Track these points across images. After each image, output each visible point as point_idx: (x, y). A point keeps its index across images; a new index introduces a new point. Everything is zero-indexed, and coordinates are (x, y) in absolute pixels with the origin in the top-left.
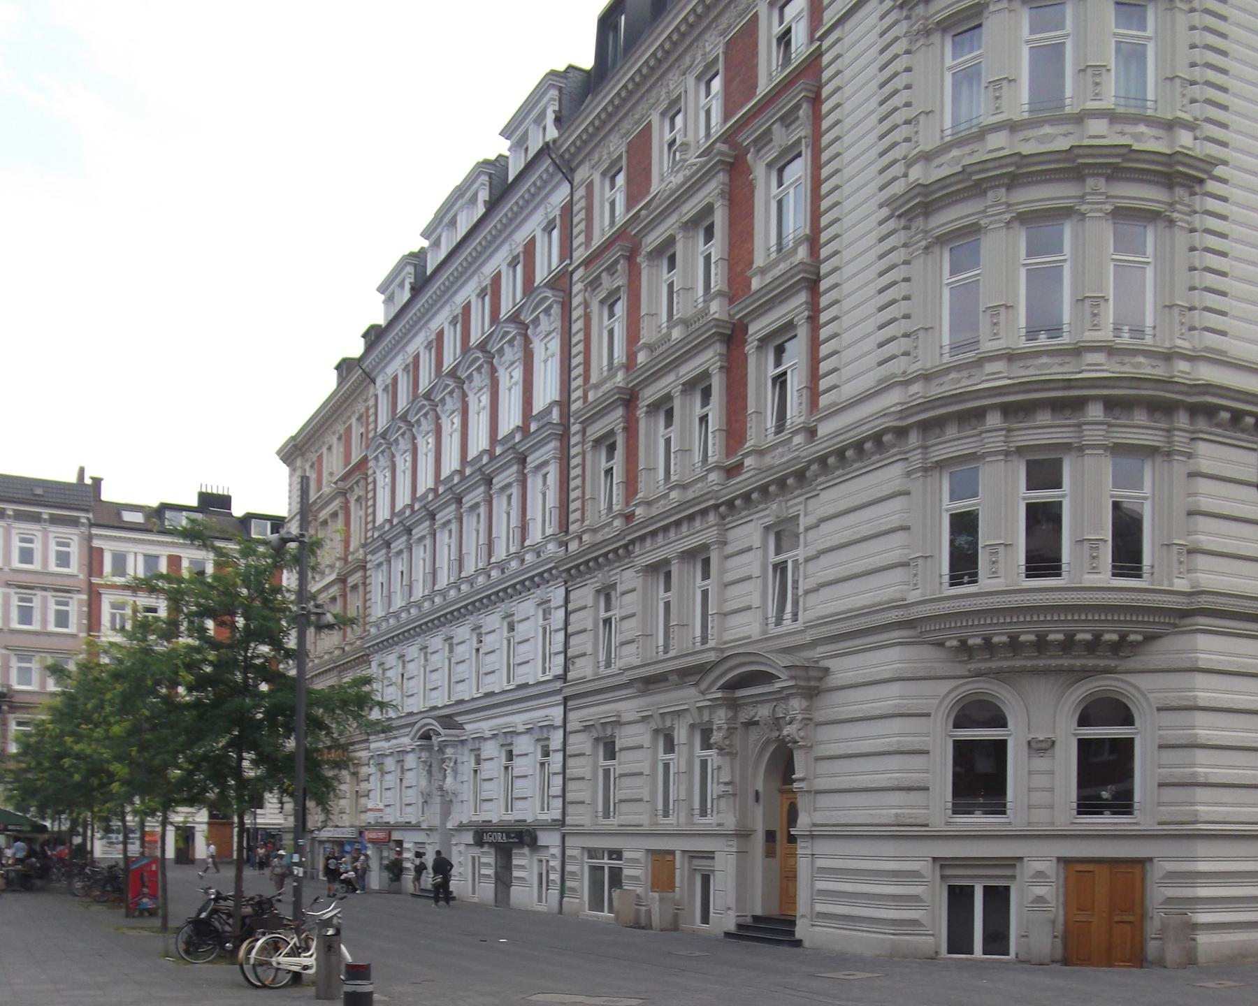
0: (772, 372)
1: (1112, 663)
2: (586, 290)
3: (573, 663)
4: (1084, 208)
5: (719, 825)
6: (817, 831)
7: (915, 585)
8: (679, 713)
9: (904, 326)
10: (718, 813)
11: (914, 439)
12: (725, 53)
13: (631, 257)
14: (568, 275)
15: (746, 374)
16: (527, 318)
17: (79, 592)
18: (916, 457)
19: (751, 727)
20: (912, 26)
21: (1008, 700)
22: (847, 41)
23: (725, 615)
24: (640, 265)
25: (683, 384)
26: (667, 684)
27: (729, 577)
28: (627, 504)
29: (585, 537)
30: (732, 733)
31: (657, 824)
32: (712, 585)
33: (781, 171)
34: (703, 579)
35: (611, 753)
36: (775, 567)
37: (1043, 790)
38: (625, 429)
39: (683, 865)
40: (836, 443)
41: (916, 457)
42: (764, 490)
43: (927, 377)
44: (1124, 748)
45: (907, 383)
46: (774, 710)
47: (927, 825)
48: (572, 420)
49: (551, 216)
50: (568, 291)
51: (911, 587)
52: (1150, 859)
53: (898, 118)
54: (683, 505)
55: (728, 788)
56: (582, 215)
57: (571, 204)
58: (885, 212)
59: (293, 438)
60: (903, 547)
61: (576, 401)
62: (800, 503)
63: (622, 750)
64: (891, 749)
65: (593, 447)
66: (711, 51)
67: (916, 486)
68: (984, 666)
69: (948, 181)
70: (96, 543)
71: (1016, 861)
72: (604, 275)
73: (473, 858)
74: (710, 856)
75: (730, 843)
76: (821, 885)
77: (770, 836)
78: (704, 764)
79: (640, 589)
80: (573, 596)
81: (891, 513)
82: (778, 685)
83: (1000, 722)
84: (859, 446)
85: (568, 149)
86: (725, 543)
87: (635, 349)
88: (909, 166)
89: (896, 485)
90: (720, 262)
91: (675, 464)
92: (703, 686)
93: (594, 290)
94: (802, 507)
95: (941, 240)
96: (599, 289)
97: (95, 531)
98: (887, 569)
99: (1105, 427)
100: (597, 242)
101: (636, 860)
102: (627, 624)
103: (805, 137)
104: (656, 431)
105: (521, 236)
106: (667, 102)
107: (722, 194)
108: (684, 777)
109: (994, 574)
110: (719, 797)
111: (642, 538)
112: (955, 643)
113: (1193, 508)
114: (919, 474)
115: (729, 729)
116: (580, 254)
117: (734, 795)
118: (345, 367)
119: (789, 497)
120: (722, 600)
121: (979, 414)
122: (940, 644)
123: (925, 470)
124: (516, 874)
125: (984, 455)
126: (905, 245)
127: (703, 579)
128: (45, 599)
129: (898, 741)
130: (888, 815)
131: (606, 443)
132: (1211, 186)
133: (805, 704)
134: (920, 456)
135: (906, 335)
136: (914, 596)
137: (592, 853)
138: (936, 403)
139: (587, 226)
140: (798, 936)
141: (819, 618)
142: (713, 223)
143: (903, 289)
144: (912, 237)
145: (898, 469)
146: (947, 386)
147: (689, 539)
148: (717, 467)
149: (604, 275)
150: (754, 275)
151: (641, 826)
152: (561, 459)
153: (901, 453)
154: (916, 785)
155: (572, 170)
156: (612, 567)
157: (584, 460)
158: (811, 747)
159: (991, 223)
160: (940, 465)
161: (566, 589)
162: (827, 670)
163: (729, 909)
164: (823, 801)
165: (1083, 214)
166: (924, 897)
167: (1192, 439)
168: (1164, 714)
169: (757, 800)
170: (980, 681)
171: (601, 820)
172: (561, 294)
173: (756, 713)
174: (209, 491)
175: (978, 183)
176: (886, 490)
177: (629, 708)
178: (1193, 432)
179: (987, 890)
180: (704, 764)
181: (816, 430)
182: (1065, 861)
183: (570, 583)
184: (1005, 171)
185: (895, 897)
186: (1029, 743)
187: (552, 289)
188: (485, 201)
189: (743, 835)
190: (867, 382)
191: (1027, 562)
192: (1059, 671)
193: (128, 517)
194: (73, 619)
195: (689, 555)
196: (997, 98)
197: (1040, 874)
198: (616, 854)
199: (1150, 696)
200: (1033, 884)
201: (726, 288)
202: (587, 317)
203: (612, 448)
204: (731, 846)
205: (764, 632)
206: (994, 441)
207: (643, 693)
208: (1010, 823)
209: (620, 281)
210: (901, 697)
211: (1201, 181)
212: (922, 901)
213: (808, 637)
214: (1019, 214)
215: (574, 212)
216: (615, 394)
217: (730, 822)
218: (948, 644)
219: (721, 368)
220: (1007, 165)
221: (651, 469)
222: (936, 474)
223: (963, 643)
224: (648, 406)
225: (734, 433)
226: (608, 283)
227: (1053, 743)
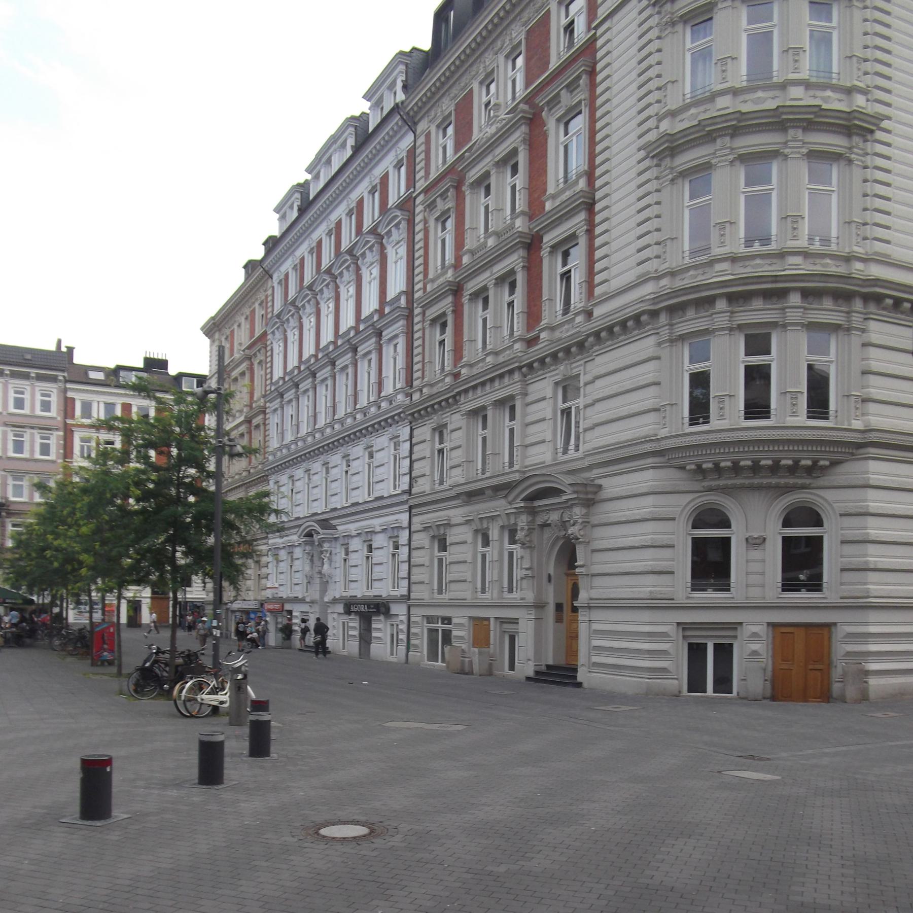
0: (560, 270)
1: (808, 481)
2: (425, 211)
3: (416, 482)
4: (786, 151)
6: (593, 603)
8: (493, 518)
9: (656, 236)
10: (521, 590)
11: (663, 319)
12: (526, 39)
13: (458, 187)
15: (542, 272)
16: (382, 231)
17: (57, 430)
18: (665, 332)
19: (545, 528)
20: (662, 19)
21: (732, 508)
22: (615, 30)
23: (526, 446)
24: (464, 192)
25: (496, 279)
26: (484, 497)
28: (455, 366)
29: (425, 390)
30: (531, 533)
31: (477, 598)
32: (517, 424)
33: (567, 124)
34: (510, 421)
35: (443, 547)
36: (563, 411)
39: (495, 628)
40: (607, 322)
41: (665, 332)
42: (554, 356)
43: (673, 274)
44: (816, 543)
45: (658, 278)
47: (673, 599)
48: (415, 305)
50: (412, 211)
51: (661, 426)
52: (835, 624)
54: (496, 367)
55: (529, 572)
57: (414, 148)
58: (642, 154)
59: (213, 318)
60: (656, 397)
62: (581, 365)
64: (646, 544)
65: (430, 324)
66: (516, 37)
67: (665, 353)
69: (688, 132)
70: (70, 394)
72: (438, 200)
73: (344, 623)
74: (515, 621)
75: (530, 612)
76: (596, 643)
77: (559, 607)
78: (511, 554)
79: (464, 427)
80: (416, 432)
81: (647, 372)
82: (564, 498)
83: (726, 524)
84: (623, 324)
85: (412, 108)
86: (526, 394)
87: (461, 253)
89: (650, 352)
90: (522, 191)
91: (490, 337)
93: (431, 210)
94: (582, 368)
95: (683, 174)
96: (435, 210)
97: (69, 386)
99: (802, 310)
100: (433, 176)
102: (455, 453)
104: (476, 313)
106: (484, 74)
107: (524, 141)
108: (496, 565)
109: (722, 417)
110: (522, 579)
111: (466, 391)
112: (693, 467)
113: (866, 369)
115: (529, 529)
116: (421, 185)
117: (533, 577)
118: (250, 266)
119: (572, 361)
120: (524, 436)
121: (710, 301)
122: (682, 468)
124: (374, 634)
125: (714, 331)
126: (657, 178)
127: (510, 421)
128: (32, 435)
130: (645, 592)
131: (440, 322)
132: (879, 135)
133: (584, 511)
134: (667, 331)
135: (658, 243)
136: (663, 433)
137: (430, 619)
138: (680, 293)
139: (426, 164)
140: (579, 679)
141: (594, 449)
142: (517, 162)
143: (655, 210)
144: (662, 172)
145: (651, 341)
146: (687, 280)
147: (500, 391)
148: (521, 339)
149: (438, 200)
150: (548, 199)
151: (465, 599)
152: (407, 333)
155: (415, 124)
158: (589, 542)
159: (719, 162)
160: (682, 338)
161: (411, 427)
162: (600, 486)
163: (529, 660)
164: (598, 581)
166: (671, 651)
167: (865, 319)
168: (845, 519)
169: (550, 581)
170: (711, 495)
171: (436, 596)
172: (407, 213)
174: (152, 356)
175: (710, 133)
176: (643, 356)
177: (457, 514)
178: (866, 314)
180: (511, 554)
181: (592, 312)
182: (773, 625)
183: (413, 424)
184: (729, 124)
185: (649, 652)
186: (747, 539)
187: (401, 210)
188: (352, 146)
189: (539, 606)
190: (630, 277)
191: (745, 408)
192: (769, 487)
193: (93, 375)
194: (53, 449)
195: (500, 403)
197: (755, 635)
198: (447, 620)
199: (835, 505)
200: (750, 642)
201: (527, 209)
202: (426, 231)
203: (444, 326)
204: (530, 614)
205: (555, 459)
206: (722, 320)
207: (467, 503)
208: (733, 598)
209: (450, 204)
210: (654, 506)
211: (872, 132)
212: (669, 654)
213: (586, 463)
218: (688, 467)
219: (523, 267)
220: (731, 120)
221: (473, 341)
222: (680, 344)
223: (699, 467)
224: (470, 295)
225: (533, 315)
226: (441, 206)
227: (764, 539)
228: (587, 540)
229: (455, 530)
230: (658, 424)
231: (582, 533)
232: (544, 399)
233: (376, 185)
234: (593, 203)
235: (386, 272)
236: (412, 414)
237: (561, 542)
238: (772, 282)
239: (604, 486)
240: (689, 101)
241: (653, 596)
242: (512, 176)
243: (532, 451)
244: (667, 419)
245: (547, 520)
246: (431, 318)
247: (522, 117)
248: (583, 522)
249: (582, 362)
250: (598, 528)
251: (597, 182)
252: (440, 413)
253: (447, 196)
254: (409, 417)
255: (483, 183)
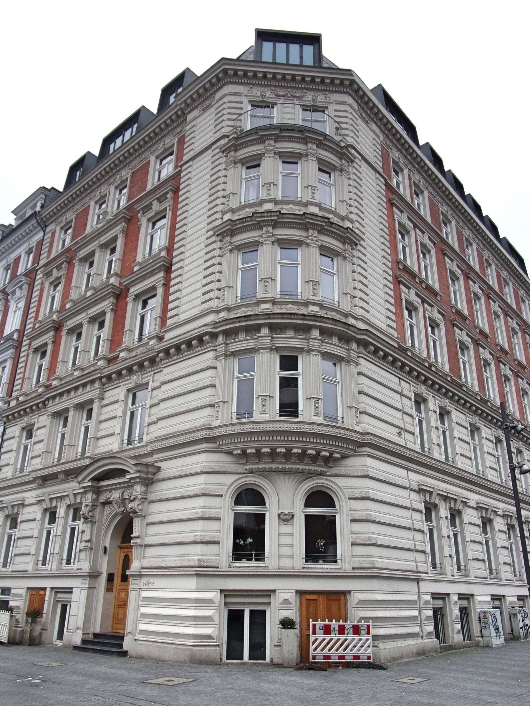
1: (325, 470)
2: (44, 277)
4: (308, 241)
5: (78, 570)
7: (217, 417)
8: (61, 498)
9: (217, 285)
10: (79, 561)
11: (221, 339)
12: (131, 177)
14: (35, 272)
15: (126, 313)
16: (9, 290)
20: (227, 160)
22: (194, 167)
23: (98, 439)
24: (74, 264)
25: (90, 318)
26: (56, 480)
27: (102, 417)
28: (48, 380)
31: (37, 570)
32: (92, 423)
33: (154, 224)
37: (286, 545)
38: (53, 342)
39: (50, 598)
40: (176, 341)
41: (221, 349)
43: (229, 309)
44: (331, 522)
45: (218, 312)
46: (123, 494)
47: (218, 567)
48: (25, 338)
49: (31, 246)
50: (33, 279)
51: (214, 419)
52: (349, 592)
53: (220, 194)
55: (88, 544)
56: (36, 304)
57: (43, 240)
58: (211, 233)
60: (211, 396)
61: (22, 357)
62: (151, 375)
63: (21, 522)
64: (197, 516)
65: (33, 352)
66: (168, 143)
67: (220, 364)
68: (254, 467)
71: (269, 593)
72: (54, 270)
74: (69, 591)
75: (84, 582)
77: (111, 577)
78: (73, 530)
79: (48, 427)
80: (7, 431)
81: (206, 377)
84: (189, 343)
85: (45, 216)
86: (103, 399)
87: (65, 302)
88: (223, 215)
89: (209, 363)
90: (117, 261)
91: (79, 358)
92: (80, 478)
93: (48, 277)
94: (151, 378)
95: (238, 248)
98: (202, 408)
99: (320, 342)
100: (53, 255)
101: (20, 595)
102: (37, 446)
103: (169, 206)
105: (14, 256)
106: (99, 196)
107: (123, 231)
108: (59, 539)
109: (264, 412)
110: (80, 551)
111: (54, 397)
112: (239, 452)
113: (361, 390)
114: (223, 357)
115: (92, 506)
116: (42, 263)
117: (91, 549)
121: (257, 328)
122: (230, 453)
123: (226, 356)
125: (259, 349)
126: (220, 248)
127: (87, 420)
129: (202, 511)
131: (41, 351)
132: (359, 247)
133: (144, 489)
134: (224, 348)
135: (219, 289)
138: (235, 320)
139: (49, 250)
140: (125, 648)
142: (116, 246)
143: (218, 268)
144: (223, 245)
145: (211, 355)
146: (241, 313)
147: (82, 397)
148: (104, 358)
149: (54, 270)
151: (26, 571)
152: (14, 359)
153: (212, 347)
154: (212, 540)
155: (46, 226)
156: (34, 414)
157: (25, 370)
158: (145, 516)
160: (234, 354)
161: (5, 427)
162: (159, 468)
163: (78, 628)
164: (150, 552)
165: (308, 244)
167: (358, 357)
168: (353, 502)
169: (105, 552)
170: (251, 476)
171: (64, 566)
172: (30, 280)
173: (111, 496)
175: (259, 223)
176: (203, 366)
177: (30, 496)
178: (358, 353)
179: (252, 612)
180: (73, 530)
182: (300, 593)
183: (7, 424)
184: (273, 218)
185: (196, 618)
186: (279, 515)
191: (280, 408)
192: (296, 472)
195: (80, 406)
196: (269, 190)
197: (286, 601)
199: (344, 490)
200: (281, 608)
202: (42, 290)
203: (44, 354)
204: (85, 583)
206: (265, 342)
207: (41, 486)
209: (62, 272)
210: (205, 484)
211: (356, 244)
213: (148, 449)
214: (278, 239)
215: (30, 312)
216: (50, 324)
217: (85, 566)
219: (112, 309)
220: (274, 216)
221: (65, 362)
222: (232, 358)
223: (244, 452)
224: (68, 330)
226: (56, 274)
227: (293, 516)
228: (144, 515)
229: (27, 510)
230: (213, 417)
231: (140, 507)
232: (117, 401)
233: (10, 264)
234: (171, 265)
235: (6, 318)
236: (7, 417)
237: (119, 518)
238: (301, 319)
239: (161, 468)
240: (243, 204)
241: (202, 564)
242: (99, 330)
243: (102, 442)
244: (220, 413)
245: (109, 498)
246: (34, 347)
247: (112, 291)
248: (142, 498)
249: (152, 373)
250: (152, 504)
251: (175, 246)
252: (30, 415)
253: (62, 268)
254: (5, 419)
255: (89, 260)
